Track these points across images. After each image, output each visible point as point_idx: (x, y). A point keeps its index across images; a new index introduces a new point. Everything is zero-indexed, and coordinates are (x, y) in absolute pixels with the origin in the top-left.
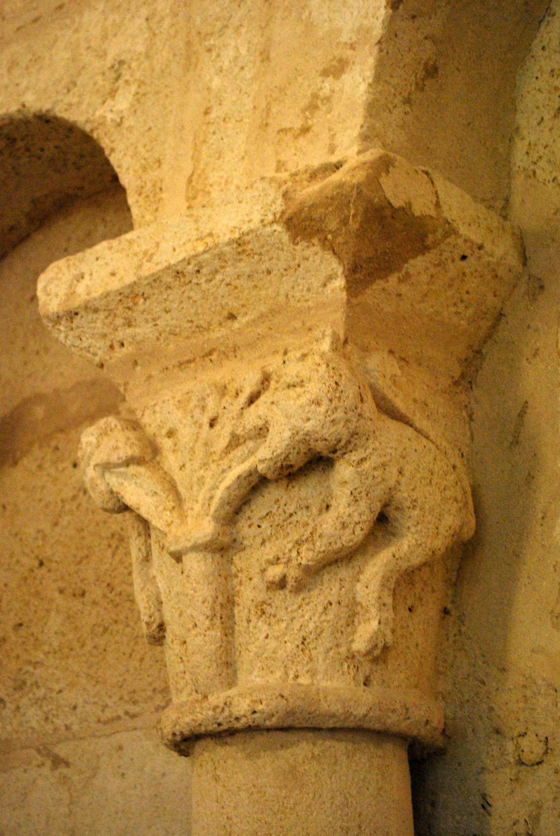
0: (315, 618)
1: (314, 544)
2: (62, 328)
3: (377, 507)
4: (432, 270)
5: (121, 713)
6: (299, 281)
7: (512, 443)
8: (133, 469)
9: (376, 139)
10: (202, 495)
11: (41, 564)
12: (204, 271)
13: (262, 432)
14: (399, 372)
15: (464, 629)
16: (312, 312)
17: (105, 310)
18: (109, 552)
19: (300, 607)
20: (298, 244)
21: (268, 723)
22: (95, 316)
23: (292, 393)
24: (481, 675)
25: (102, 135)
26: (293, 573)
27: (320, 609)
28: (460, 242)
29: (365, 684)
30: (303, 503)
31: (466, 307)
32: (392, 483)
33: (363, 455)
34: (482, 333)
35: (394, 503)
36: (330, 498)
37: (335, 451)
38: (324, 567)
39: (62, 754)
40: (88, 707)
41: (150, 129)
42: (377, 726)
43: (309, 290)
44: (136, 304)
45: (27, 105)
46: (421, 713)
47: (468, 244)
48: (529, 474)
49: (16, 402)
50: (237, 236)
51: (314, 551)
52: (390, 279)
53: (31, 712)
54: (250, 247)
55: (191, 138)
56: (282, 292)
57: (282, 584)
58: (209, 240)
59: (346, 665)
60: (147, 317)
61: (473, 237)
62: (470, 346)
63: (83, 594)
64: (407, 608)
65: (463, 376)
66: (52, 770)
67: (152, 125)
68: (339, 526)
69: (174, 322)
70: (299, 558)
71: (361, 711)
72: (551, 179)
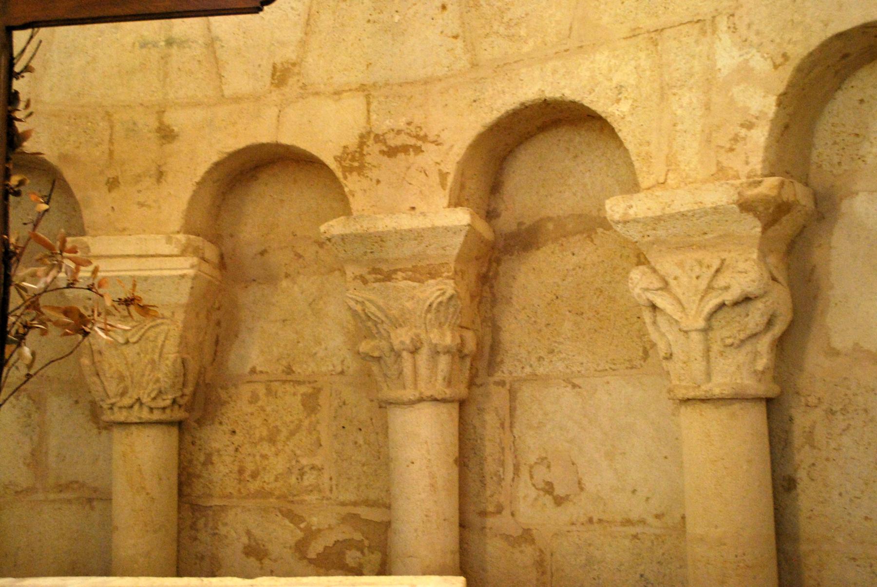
8: (659, 292)
26: (737, 342)
46: (773, 390)
49: (537, 218)
53: (559, 364)
57: (732, 345)
63: (582, 313)
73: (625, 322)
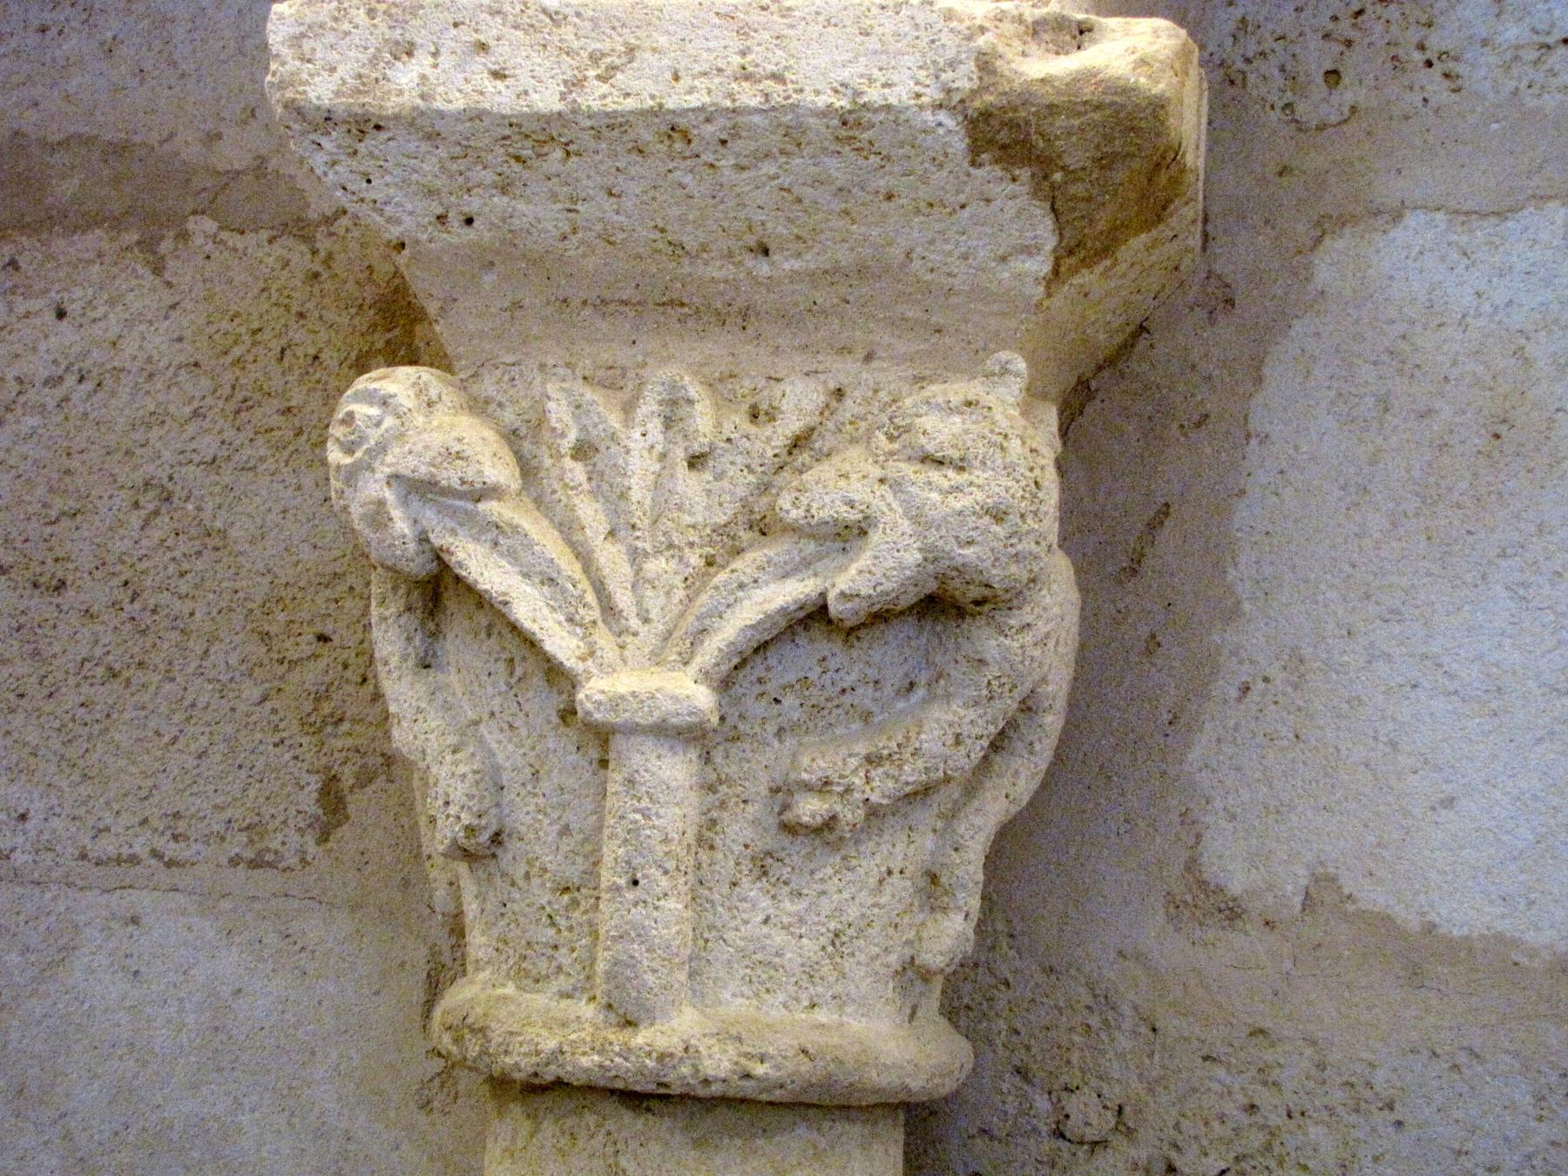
1: (900, 767)
12: (737, 145)
16: (954, 300)
18: (136, 519)
20: (981, 165)
22: (425, 147)
27: (872, 881)
30: (872, 673)
43: (965, 257)
48: (1153, 636)
51: (897, 781)
56: (903, 243)
60: (557, 188)
63: (61, 585)
68: (950, 740)
69: (622, 218)
70: (867, 789)
72: (1280, 104)
73: (258, 651)
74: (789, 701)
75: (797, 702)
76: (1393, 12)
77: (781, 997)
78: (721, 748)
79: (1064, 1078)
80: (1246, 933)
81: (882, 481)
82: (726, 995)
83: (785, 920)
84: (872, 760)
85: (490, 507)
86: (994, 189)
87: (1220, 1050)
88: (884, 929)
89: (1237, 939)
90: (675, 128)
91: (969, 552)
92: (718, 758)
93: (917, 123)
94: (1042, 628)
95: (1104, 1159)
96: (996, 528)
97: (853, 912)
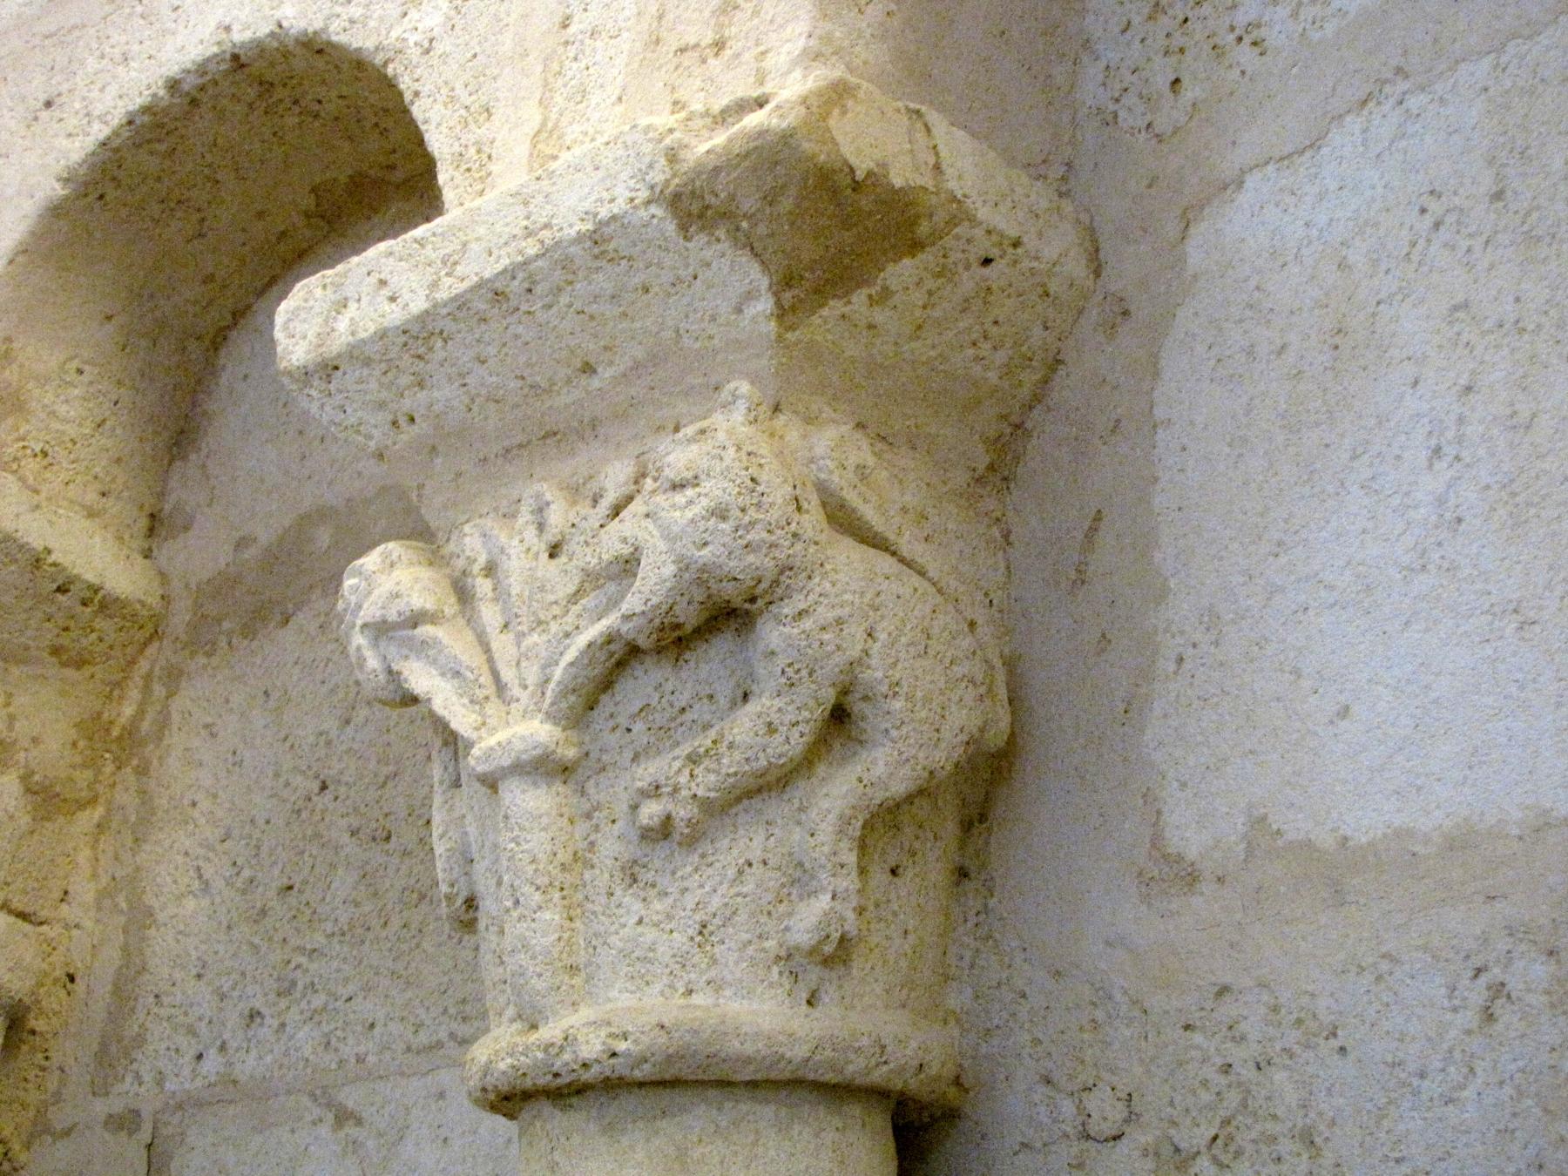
0: (722, 890)
2: (314, 393)
3: (829, 696)
4: (930, 284)
5: (443, 1035)
6: (697, 304)
7: (1074, 582)
9: (835, 58)
10: (532, 674)
11: (324, 787)
12: (538, 290)
13: (627, 566)
14: (871, 461)
15: (992, 902)
17: (381, 361)
19: (696, 870)
21: (637, 1074)
22: (366, 372)
23: (680, 498)
24: (1020, 983)
25: (401, 69)
26: (683, 812)
28: (979, 232)
29: (809, 1002)
31: (995, 348)
32: (854, 652)
33: (802, 606)
34: (1025, 392)
35: (860, 689)
36: (749, 681)
37: (753, 600)
38: (738, 800)
39: (350, 1104)
40: (392, 1026)
41: (475, 56)
42: (830, 1077)
43: (713, 319)
44: (431, 349)
45: (285, 24)
47: (994, 238)
48: (1104, 636)
50: (590, 227)
52: (854, 299)
54: (612, 246)
55: (540, 68)
58: (545, 234)
59: (775, 970)
61: (1002, 225)
62: (1004, 417)
64: (887, 868)
65: (991, 467)
66: (334, 1131)
67: (478, 50)
69: (494, 379)
71: (800, 1052)
74: (638, 727)
75: (644, 728)
76: (1206, 9)
77: (657, 987)
78: (592, 781)
79: (1082, 1078)
80: (1202, 894)
81: (647, 516)
82: (614, 994)
83: (655, 918)
84: (693, 759)
85: (426, 630)
86: (708, 254)
87: (1195, 1017)
88: (752, 915)
89: (1196, 901)
90: (495, 292)
91: (705, 552)
92: (591, 791)
93: (635, 220)
94: (825, 614)
95: (1123, 1147)
96: (723, 526)
97: (716, 903)
